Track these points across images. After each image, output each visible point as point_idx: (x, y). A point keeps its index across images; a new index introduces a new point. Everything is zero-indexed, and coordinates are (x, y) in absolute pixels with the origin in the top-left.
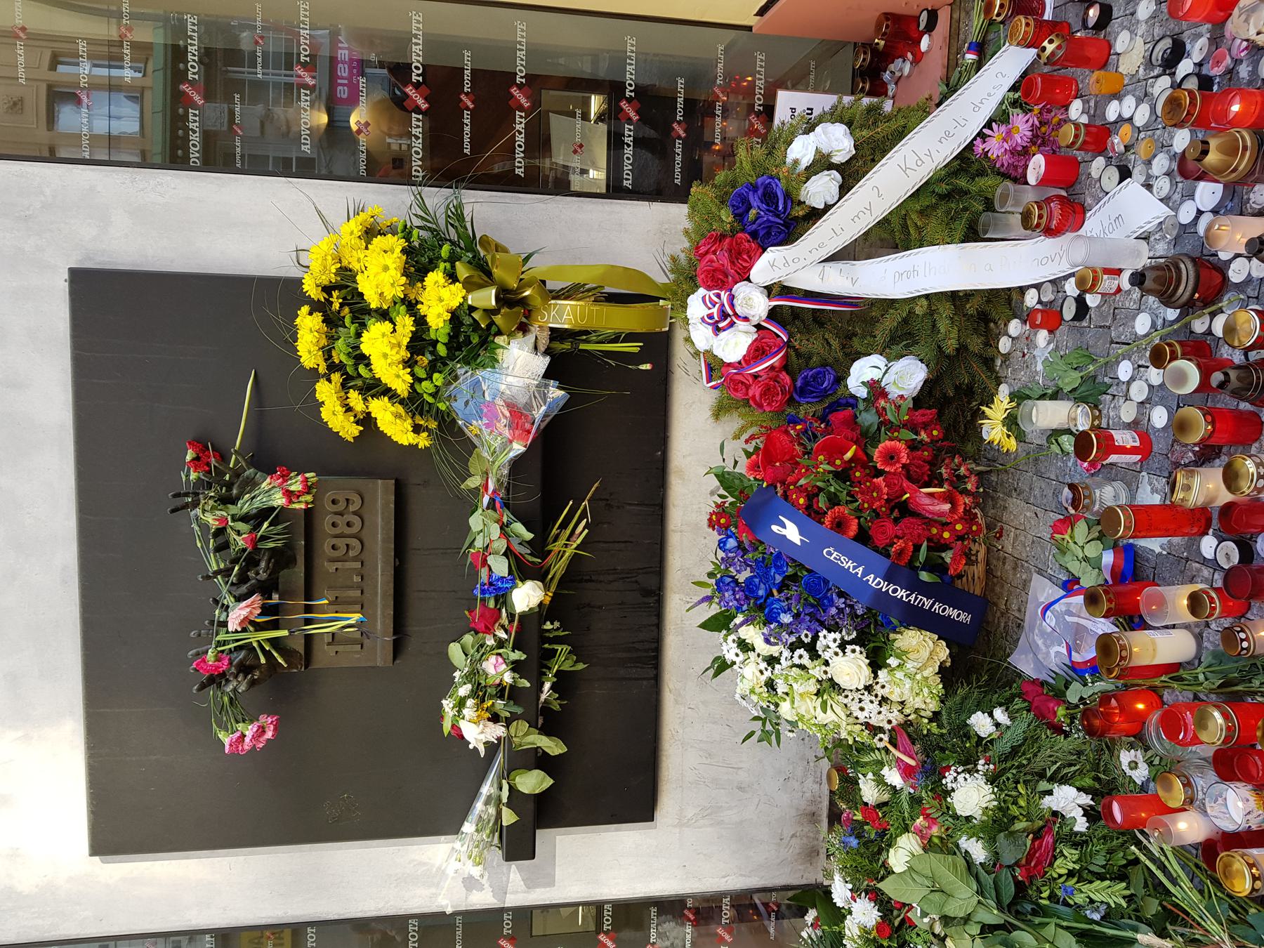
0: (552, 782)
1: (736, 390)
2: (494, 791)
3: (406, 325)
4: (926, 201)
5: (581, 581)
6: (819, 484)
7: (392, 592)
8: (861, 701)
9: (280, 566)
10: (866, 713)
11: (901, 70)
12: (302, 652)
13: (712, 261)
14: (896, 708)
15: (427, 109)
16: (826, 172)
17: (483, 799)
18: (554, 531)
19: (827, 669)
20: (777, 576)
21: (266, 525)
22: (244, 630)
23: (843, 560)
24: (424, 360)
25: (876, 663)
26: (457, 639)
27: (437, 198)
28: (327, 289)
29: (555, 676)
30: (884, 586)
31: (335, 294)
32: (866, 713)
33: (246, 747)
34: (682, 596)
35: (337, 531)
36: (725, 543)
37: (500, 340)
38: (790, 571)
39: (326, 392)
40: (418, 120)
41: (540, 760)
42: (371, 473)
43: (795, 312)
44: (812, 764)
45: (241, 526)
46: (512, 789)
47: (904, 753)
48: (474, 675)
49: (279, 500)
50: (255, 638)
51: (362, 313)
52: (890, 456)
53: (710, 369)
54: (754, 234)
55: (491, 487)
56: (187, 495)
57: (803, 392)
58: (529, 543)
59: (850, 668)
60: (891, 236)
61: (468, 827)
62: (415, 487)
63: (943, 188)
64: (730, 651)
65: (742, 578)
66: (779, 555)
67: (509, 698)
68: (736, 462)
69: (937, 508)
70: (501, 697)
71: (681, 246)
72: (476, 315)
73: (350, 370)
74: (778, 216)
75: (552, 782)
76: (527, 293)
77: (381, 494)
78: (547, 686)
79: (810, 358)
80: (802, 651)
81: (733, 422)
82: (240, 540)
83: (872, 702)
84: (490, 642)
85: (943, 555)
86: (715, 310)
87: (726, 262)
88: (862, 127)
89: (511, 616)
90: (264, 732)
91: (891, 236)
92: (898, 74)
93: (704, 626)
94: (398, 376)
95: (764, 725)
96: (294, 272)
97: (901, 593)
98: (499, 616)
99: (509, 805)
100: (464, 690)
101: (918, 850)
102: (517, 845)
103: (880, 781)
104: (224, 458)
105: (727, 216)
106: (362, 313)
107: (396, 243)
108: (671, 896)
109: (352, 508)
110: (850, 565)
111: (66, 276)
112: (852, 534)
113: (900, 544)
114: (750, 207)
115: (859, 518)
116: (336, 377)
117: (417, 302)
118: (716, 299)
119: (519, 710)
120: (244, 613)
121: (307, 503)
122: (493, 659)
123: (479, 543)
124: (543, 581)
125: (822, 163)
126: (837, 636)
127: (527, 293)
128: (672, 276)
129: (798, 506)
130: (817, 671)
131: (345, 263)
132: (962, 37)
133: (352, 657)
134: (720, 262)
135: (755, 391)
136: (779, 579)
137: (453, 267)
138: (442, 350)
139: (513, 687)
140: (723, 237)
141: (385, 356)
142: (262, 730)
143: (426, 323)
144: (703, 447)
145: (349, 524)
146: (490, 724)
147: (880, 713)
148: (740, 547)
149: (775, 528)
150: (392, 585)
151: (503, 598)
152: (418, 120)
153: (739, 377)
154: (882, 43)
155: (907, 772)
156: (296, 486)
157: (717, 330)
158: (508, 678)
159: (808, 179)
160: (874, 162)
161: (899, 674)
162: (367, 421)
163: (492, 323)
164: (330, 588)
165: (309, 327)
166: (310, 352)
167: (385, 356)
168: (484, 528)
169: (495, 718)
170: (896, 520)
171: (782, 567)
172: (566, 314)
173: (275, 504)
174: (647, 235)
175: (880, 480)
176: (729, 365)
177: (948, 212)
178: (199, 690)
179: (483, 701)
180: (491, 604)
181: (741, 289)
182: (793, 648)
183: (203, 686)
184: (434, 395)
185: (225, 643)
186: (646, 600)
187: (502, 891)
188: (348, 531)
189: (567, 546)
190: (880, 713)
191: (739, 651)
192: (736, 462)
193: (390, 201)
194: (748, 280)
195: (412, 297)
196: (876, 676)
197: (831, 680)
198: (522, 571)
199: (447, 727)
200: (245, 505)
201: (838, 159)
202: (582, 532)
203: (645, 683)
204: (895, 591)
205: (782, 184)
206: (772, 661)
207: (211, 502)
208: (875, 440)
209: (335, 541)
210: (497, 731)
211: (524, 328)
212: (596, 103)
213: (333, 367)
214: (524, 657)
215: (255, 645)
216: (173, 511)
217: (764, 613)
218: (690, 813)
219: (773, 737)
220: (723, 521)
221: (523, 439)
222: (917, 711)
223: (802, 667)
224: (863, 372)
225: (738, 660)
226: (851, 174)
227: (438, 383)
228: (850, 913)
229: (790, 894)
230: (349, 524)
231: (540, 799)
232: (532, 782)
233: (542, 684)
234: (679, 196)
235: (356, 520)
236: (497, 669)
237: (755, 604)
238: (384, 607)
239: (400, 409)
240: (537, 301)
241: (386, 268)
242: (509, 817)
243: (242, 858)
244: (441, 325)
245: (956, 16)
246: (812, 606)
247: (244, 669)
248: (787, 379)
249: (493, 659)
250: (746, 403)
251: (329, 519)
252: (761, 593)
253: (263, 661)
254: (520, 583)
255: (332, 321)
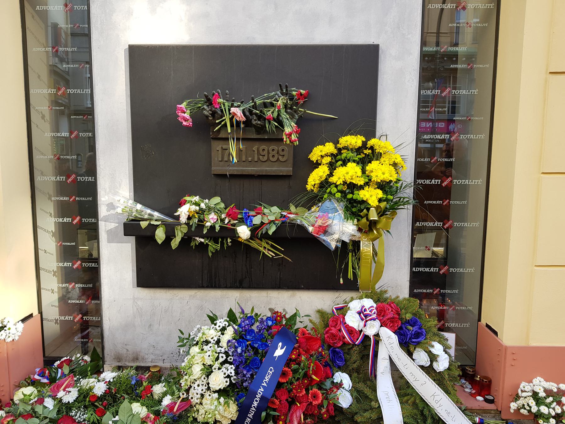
0: (160, 243)
1: (333, 321)
2: (155, 217)
3: (361, 182)
4: (421, 406)
5: (246, 253)
6: (302, 364)
7: (244, 174)
8: (203, 385)
9: (257, 129)
10: (196, 387)
11: (467, 387)
12: (219, 136)
13: (389, 310)
14: (198, 401)
15: (442, 186)
16: (429, 360)
17: (152, 213)
18: (270, 242)
19: (217, 369)
20: (257, 345)
21: (276, 124)
22: (230, 114)
23: (269, 376)
24: (345, 188)
25: (221, 392)
26: (222, 201)
27: (409, 193)
28: (372, 148)
29: (207, 244)
30: (259, 396)
31: (370, 151)
32: (196, 387)
33: (180, 114)
34: (238, 297)
35: (271, 151)
36: (270, 320)
37: (356, 220)
38: (260, 351)
39: (329, 148)
40: (438, 182)
41: (170, 236)
42: (295, 165)
43: (368, 347)
44: (161, 358)
45: (275, 115)
46: (158, 226)
47: (179, 406)
48: (209, 209)
49: (288, 130)
50: (227, 118)
51: (364, 162)
52: (315, 396)
53: (342, 308)
54: (401, 328)
55: (291, 216)
56: (287, 90)
57: (334, 352)
58: (267, 233)
59: (219, 380)
60: (403, 387)
61: (139, 206)
62: (290, 185)
63: (426, 412)
64: (221, 323)
65: (254, 328)
66: (267, 346)
67: (198, 224)
68: (301, 322)
69: (295, 419)
70: (199, 221)
71: (391, 294)
72: (365, 210)
73: (339, 157)
74: (410, 339)
75: (160, 243)
76: (375, 232)
77: (287, 169)
78: (202, 240)
79: (348, 354)
80: (225, 358)
81: (316, 319)
82: (269, 113)
83: (202, 390)
84: (223, 216)
85: (271, 421)
86: (368, 312)
87: (389, 316)
88: (448, 374)
89: (234, 225)
90: (185, 121)
91: (403, 387)
92: (464, 386)
93: (231, 311)
94: (339, 178)
95: (187, 339)
96: (378, 134)
97: (255, 404)
98: (234, 220)
99: (150, 224)
100: (203, 206)
101: (141, 416)
102: (131, 227)
103: (165, 394)
104: (302, 106)
105: (409, 316)
106: (364, 162)
107: (394, 178)
108: (101, 295)
109: (280, 157)
110: (267, 379)
111: (375, 43)
112: (280, 380)
113: (277, 402)
114: (413, 326)
115: (287, 383)
116: (335, 152)
117: (369, 185)
118: (373, 312)
119: (193, 229)
120: (239, 115)
121: (286, 141)
122: (215, 217)
123: (266, 211)
124: (250, 238)
125: (433, 358)
126: (233, 374)
127: (375, 232)
128: (379, 290)
129: (291, 355)
130: (217, 365)
131: (383, 155)
132: (484, 415)
133: (216, 157)
134: (388, 313)
135: (334, 330)
136: (256, 346)
137: (384, 201)
138: (350, 196)
139: (203, 226)
140: (399, 314)
141: (347, 173)
142: (186, 120)
143: (360, 190)
144: (305, 305)
145: (273, 156)
146: (187, 217)
147: (197, 394)
148: (270, 328)
149: (280, 344)
150: (247, 174)
151: (243, 221)
152: (438, 182)
153: (339, 322)
154: (478, 379)
155: (171, 407)
156: (293, 137)
157: (359, 313)
158: (208, 224)
159: (426, 352)
160: (434, 380)
161: (216, 403)
162: (317, 165)
163: (362, 218)
164: (246, 148)
165: (356, 141)
166: (347, 141)
167: (347, 173)
168: (272, 214)
169: (189, 218)
170: (287, 400)
171: (262, 347)
172: (366, 248)
173: (286, 128)
174: (396, 280)
175: (304, 392)
176: (344, 318)
177: (416, 415)
178: (205, 95)
179: (197, 213)
180: (239, 216)
181: (377, 323)
182: (226, 353)
183: (206, 96)
184: (330, 193)
185: (224, 105)
186: (238, 282)
187: (106, 219)
188: (271, 155)
189: (266, 249)
190: (197, 394)
191: (221, 327)
192: (301, 322)
193: (408, 173)
194: (381, 326)
195: (371, 184)
196: (215, 392)
197: (212, 372)
198: (254, 230)
199: (187, 198)
200: (284, 116)
201: (435, 365)
202: (270, 254)
203: (201, 282)
204: (257, 401)
205: (423, 341)
206: (218, 342)
207: (285, 102)
208: (320, 388)
209: (266, 150)
210: (183, 219)
211: (360, 230)
212: (440, 250)
213: (340, 150)
214: (217, 231)
215: (224, 118)
216: (280, 85)
217: (240, 337)
218: (139, 303)
219: (181, 344)
220: (279, 318)
221: (315, 231)
222: (198, 411)
223: (217, 359)
224: (342, 378)
225: (217, 327)
226: (429, 370)
227: (336, 195)
228: (99, 381)
229: (99, 350)
230: (273, 156)
231: (152, 238)
232: (160, 235)
233: (203, 238)
234: (412, 294)
235: (275, 159)
236: (211, 219)
237: (243, 334)
238: (237, 170)
239: (324, 179)
240: (371, 236)
241: (383, 174)
242: (144, 224)
243: (125, 108)
244: (361, 196)
245: (492, 412)
246: (246, 362)
247: (214, 114)
248: (339, 345)
249: (215, 217)
250: (327, 325)
251: (276, 148)
252: (248, 337)
253: (217, 121)
254: (249, 229)
255: (358, 150)
